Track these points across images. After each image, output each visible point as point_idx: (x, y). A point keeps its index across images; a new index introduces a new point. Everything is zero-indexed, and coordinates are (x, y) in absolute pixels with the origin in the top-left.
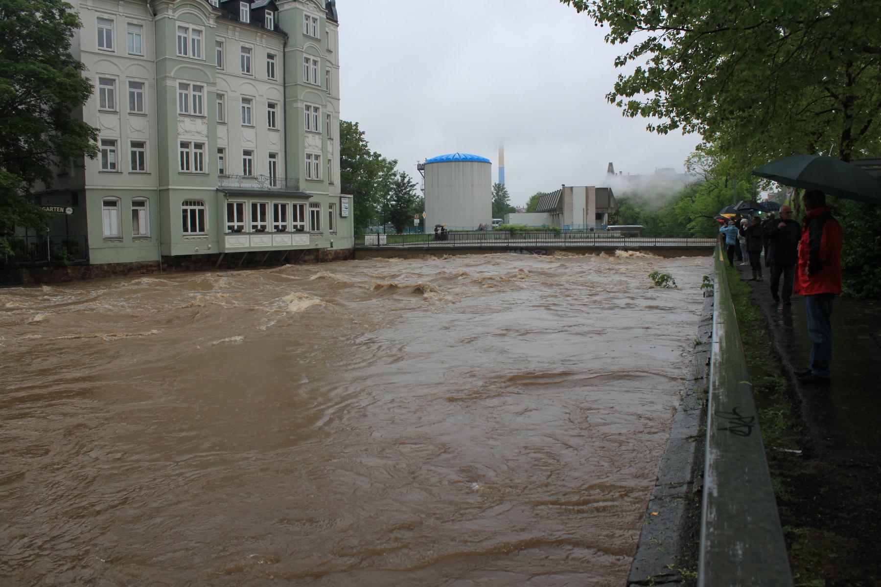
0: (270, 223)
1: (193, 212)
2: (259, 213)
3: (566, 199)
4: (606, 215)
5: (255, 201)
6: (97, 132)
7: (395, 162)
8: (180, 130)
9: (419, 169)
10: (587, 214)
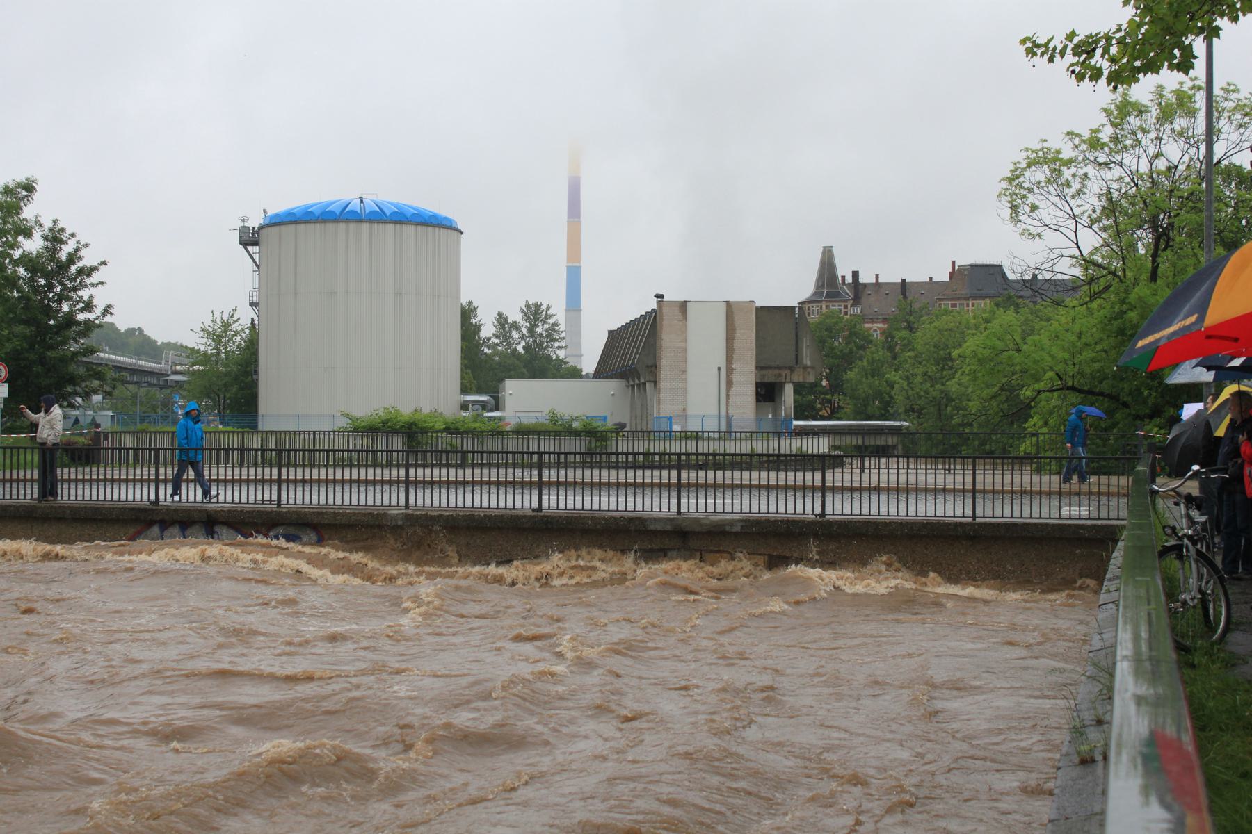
3: (668, 339)
4: (789, 390)
7: (29, 187)
9: (245, 243)
10: (729, 383)
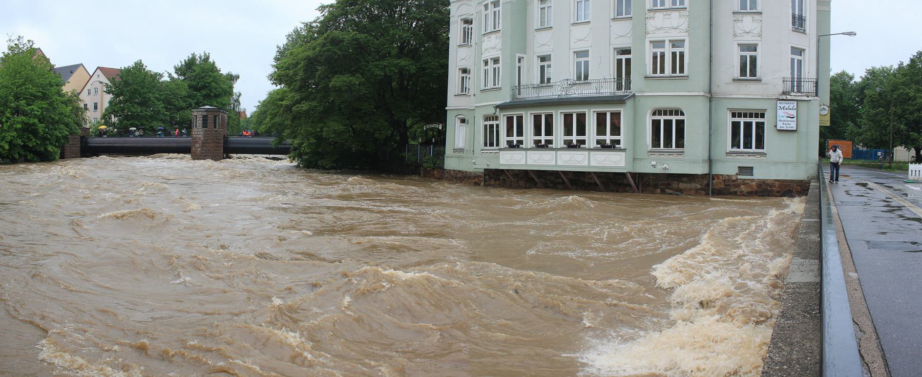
0: (529, 137)
1: (748, 126)
2: (544, 126)
5: (601, 109)
8: (650, 28)
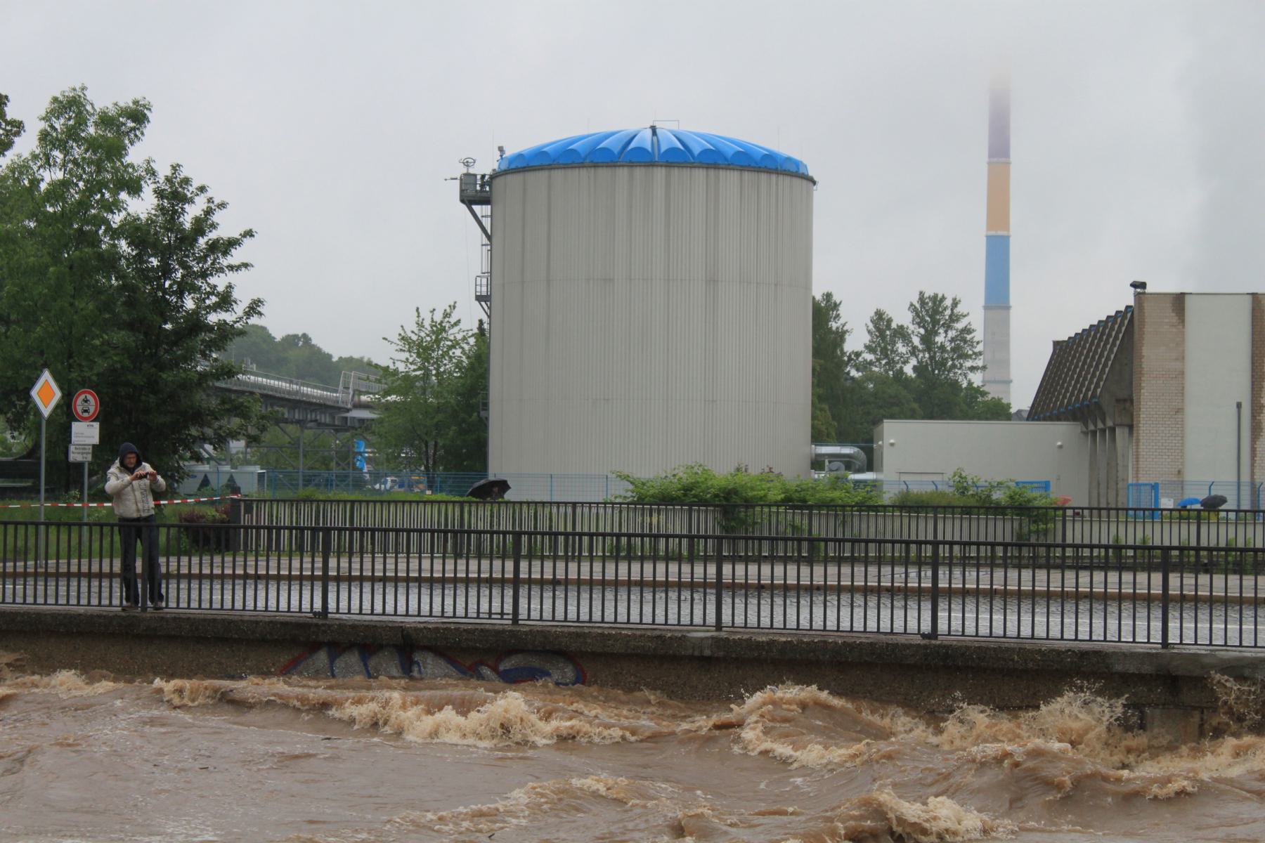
3: (1151, 354)
6: (871, 326)
7: (138, 115)
9: (470, 199)
